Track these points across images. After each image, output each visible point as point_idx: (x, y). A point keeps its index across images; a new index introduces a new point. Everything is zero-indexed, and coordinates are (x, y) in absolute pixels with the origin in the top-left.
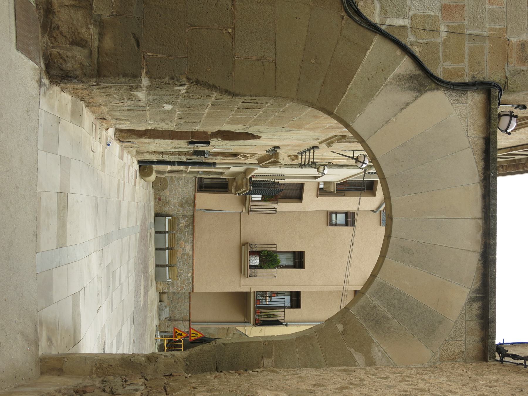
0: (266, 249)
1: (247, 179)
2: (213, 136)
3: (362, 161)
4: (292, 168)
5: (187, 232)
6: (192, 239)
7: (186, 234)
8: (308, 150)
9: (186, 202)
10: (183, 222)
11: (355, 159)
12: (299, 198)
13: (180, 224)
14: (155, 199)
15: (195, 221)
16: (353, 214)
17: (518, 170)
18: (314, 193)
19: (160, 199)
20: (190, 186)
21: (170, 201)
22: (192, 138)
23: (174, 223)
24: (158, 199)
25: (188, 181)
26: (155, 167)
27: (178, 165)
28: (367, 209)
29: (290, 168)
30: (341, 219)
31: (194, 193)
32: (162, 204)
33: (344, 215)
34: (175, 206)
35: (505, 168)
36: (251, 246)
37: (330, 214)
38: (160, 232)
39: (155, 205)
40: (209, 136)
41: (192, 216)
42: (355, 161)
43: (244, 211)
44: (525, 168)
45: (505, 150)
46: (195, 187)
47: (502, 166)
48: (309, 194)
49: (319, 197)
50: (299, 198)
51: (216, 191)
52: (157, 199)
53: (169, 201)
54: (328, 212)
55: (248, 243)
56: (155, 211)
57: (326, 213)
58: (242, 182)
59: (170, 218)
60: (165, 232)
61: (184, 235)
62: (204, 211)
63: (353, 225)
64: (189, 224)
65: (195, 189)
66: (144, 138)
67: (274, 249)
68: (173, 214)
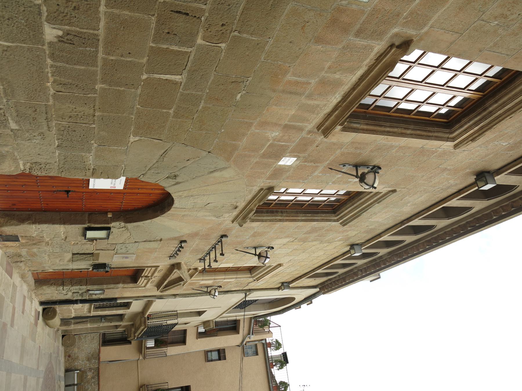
0: (158, 388)
1: (145, 318)
2: (115, 219)
3: (265, 256)
4: (185, 297)
5: (93, 382)
6: (97, 388)
7: (93, 385)
8: (213, 248)
9: (92, 355)
10: (90, 375)
11: (257, 255)
12: (183, 342)
13: (87, 376)
14: (65, 356)
15: (100, 372)
16: (224, 350)
17: (378, 267)
18: (195, 336)
19: (69, 356)
20: (95, 341)
21: (79, 356)
22: (89, 223)
23: (82, 375)
24: (68, 356)
25: (94, 337)
26: (58, 308)
27: (81, 303)
28: (234, 345)
29: (184, 297)
30: (215, 355)
31: (99, 347)
32: (72, 360)
33: (217, 353)
34: (82, 361)
35: (363, 271)
36: (148, 386)
37: (207, 352)
38: (70, 385)
39: (65, 362)
40: (110, 220)
41: (98, 368)
42: (257, 257)
43: (141, 358)
44: (387, 263)
45: (394, 228)
46: (100, 342)
47: (361, 269)
48: (191, 337)
49: (199, 339)
50: (183, 342)
51: (118, 344)
52: (67, 357)
53: (78, 357)
54: (205, 351)
55: (145, 385)
56: (65, 368)
57: (203, 352)
58: (141, 322)
59: (78, 371)
60: (74, 385)
61: (91, 385)
62: (107, 363)
63: (225, 359)
64: (95, 375)
65: (100, 344)
66: (27, 224)
67: (166, 387)
68: (81, 368)
